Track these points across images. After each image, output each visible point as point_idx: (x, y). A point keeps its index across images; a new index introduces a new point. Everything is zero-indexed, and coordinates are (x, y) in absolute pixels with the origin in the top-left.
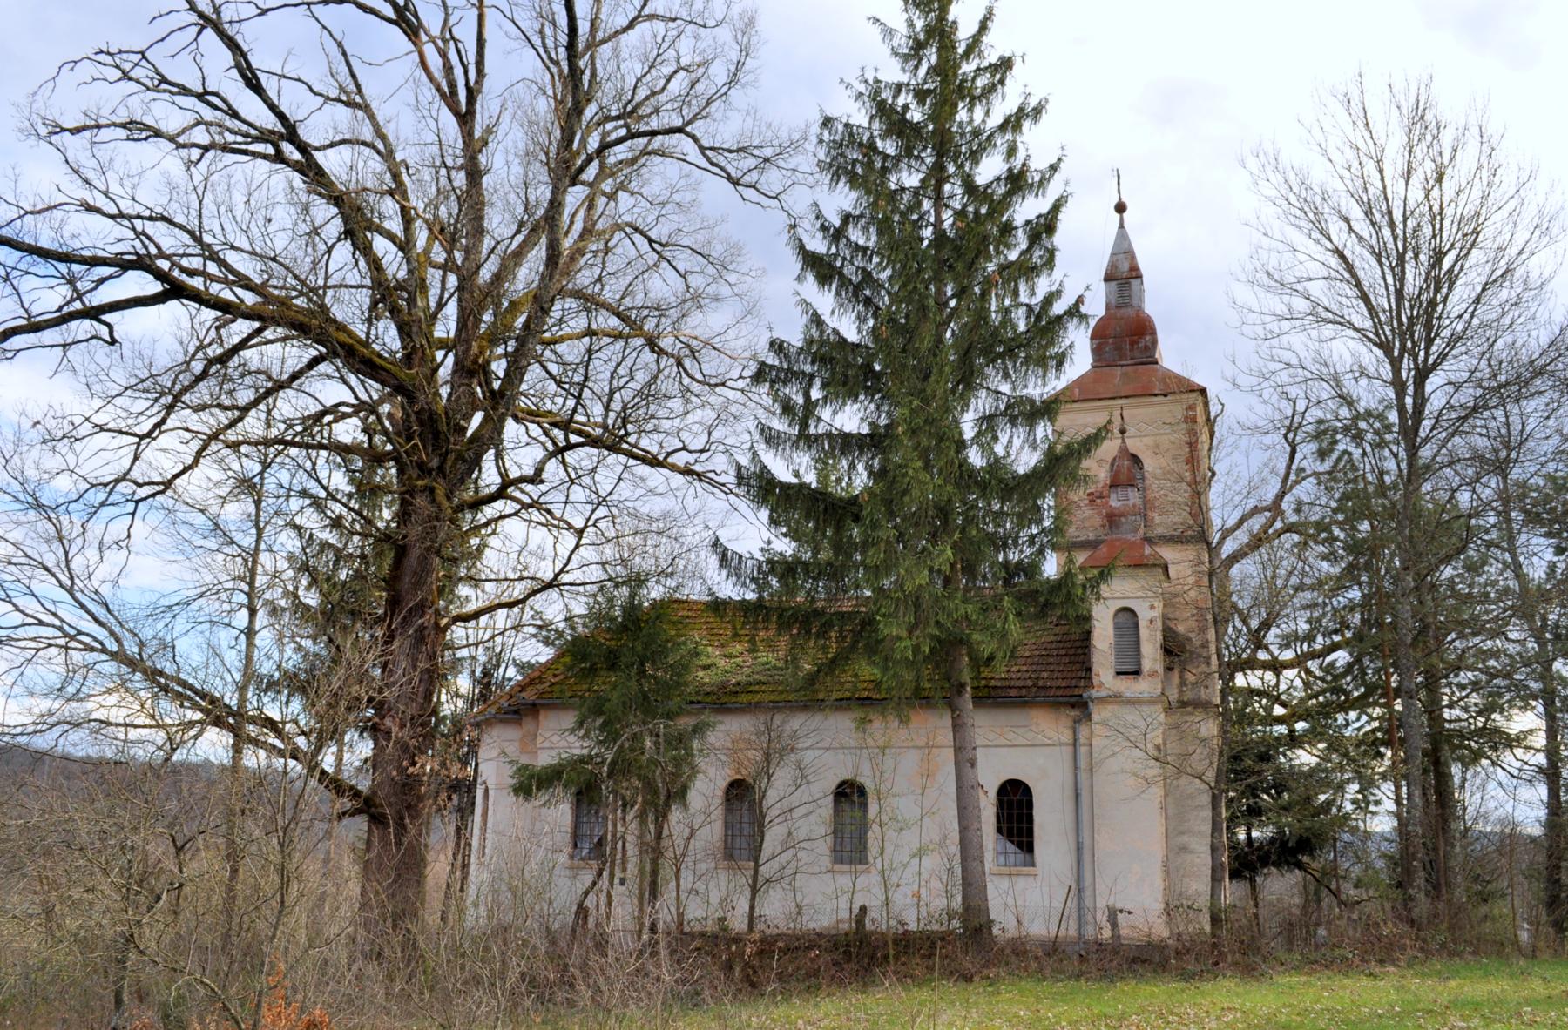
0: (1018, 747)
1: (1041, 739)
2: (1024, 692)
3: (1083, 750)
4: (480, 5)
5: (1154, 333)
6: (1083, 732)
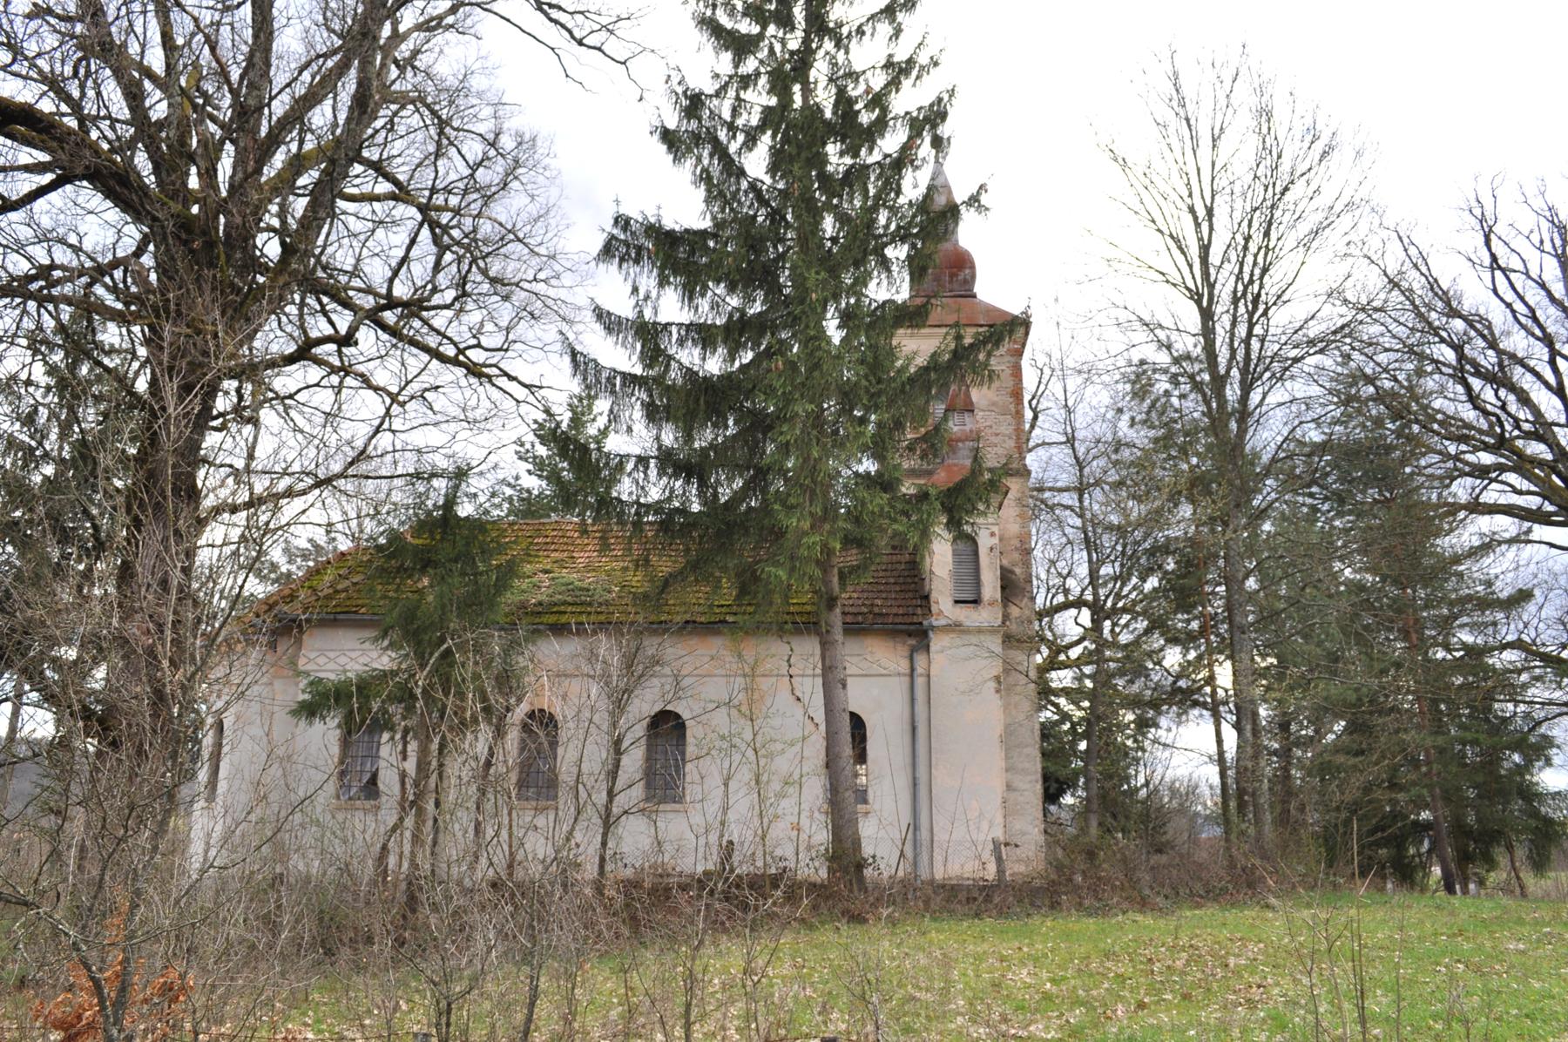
0: (875, 679)
1: (876, 669)
2: (860, 618)
3: (920, 682)
4: (3, 169)
5: (973, 267)
6: (920, 660)
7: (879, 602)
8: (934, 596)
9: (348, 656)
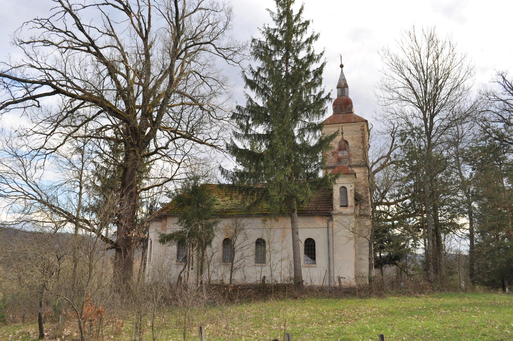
0: (311, 229)
1: (318, 226)
3: (330, 229)
5: (352, 104)
7: (319, 207)
8: (334, 205)
9: (173, 226)
